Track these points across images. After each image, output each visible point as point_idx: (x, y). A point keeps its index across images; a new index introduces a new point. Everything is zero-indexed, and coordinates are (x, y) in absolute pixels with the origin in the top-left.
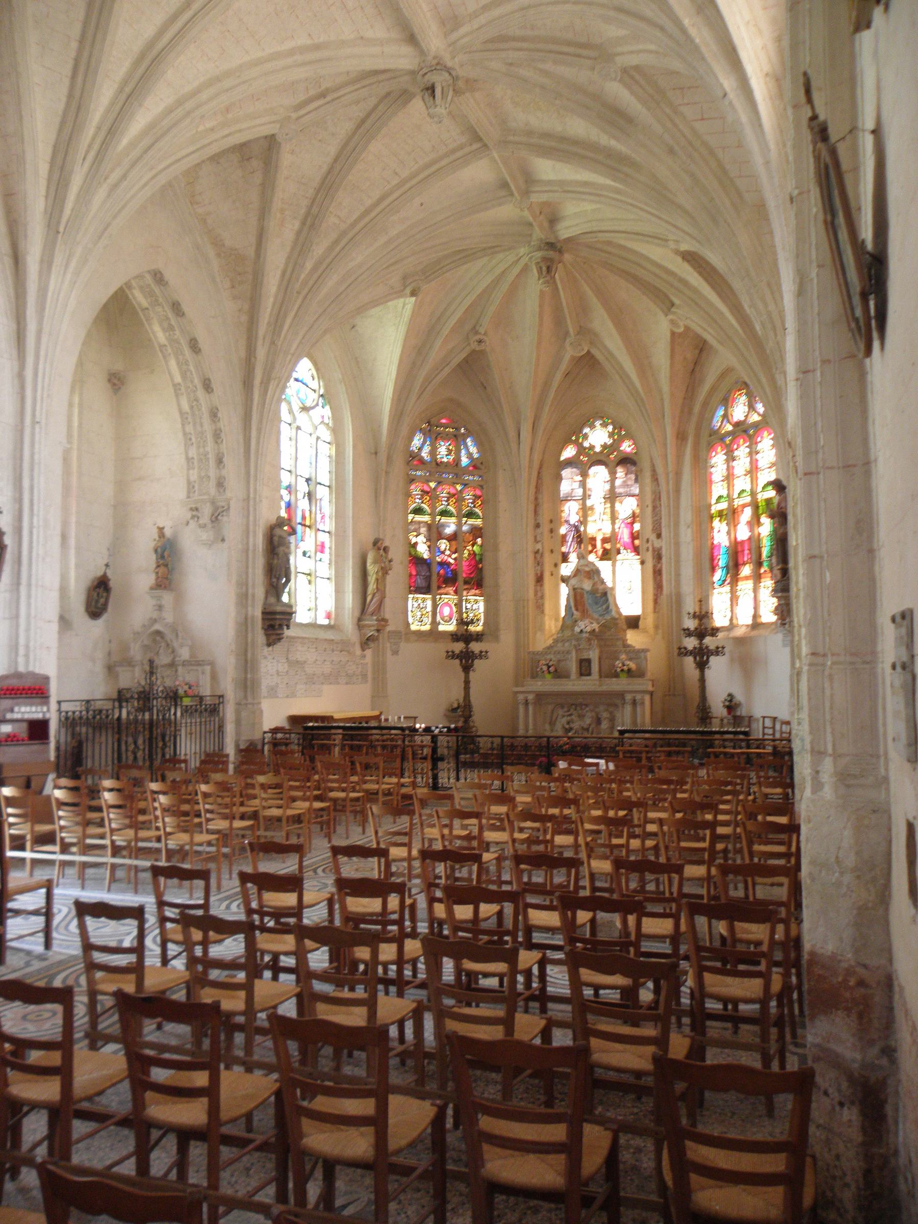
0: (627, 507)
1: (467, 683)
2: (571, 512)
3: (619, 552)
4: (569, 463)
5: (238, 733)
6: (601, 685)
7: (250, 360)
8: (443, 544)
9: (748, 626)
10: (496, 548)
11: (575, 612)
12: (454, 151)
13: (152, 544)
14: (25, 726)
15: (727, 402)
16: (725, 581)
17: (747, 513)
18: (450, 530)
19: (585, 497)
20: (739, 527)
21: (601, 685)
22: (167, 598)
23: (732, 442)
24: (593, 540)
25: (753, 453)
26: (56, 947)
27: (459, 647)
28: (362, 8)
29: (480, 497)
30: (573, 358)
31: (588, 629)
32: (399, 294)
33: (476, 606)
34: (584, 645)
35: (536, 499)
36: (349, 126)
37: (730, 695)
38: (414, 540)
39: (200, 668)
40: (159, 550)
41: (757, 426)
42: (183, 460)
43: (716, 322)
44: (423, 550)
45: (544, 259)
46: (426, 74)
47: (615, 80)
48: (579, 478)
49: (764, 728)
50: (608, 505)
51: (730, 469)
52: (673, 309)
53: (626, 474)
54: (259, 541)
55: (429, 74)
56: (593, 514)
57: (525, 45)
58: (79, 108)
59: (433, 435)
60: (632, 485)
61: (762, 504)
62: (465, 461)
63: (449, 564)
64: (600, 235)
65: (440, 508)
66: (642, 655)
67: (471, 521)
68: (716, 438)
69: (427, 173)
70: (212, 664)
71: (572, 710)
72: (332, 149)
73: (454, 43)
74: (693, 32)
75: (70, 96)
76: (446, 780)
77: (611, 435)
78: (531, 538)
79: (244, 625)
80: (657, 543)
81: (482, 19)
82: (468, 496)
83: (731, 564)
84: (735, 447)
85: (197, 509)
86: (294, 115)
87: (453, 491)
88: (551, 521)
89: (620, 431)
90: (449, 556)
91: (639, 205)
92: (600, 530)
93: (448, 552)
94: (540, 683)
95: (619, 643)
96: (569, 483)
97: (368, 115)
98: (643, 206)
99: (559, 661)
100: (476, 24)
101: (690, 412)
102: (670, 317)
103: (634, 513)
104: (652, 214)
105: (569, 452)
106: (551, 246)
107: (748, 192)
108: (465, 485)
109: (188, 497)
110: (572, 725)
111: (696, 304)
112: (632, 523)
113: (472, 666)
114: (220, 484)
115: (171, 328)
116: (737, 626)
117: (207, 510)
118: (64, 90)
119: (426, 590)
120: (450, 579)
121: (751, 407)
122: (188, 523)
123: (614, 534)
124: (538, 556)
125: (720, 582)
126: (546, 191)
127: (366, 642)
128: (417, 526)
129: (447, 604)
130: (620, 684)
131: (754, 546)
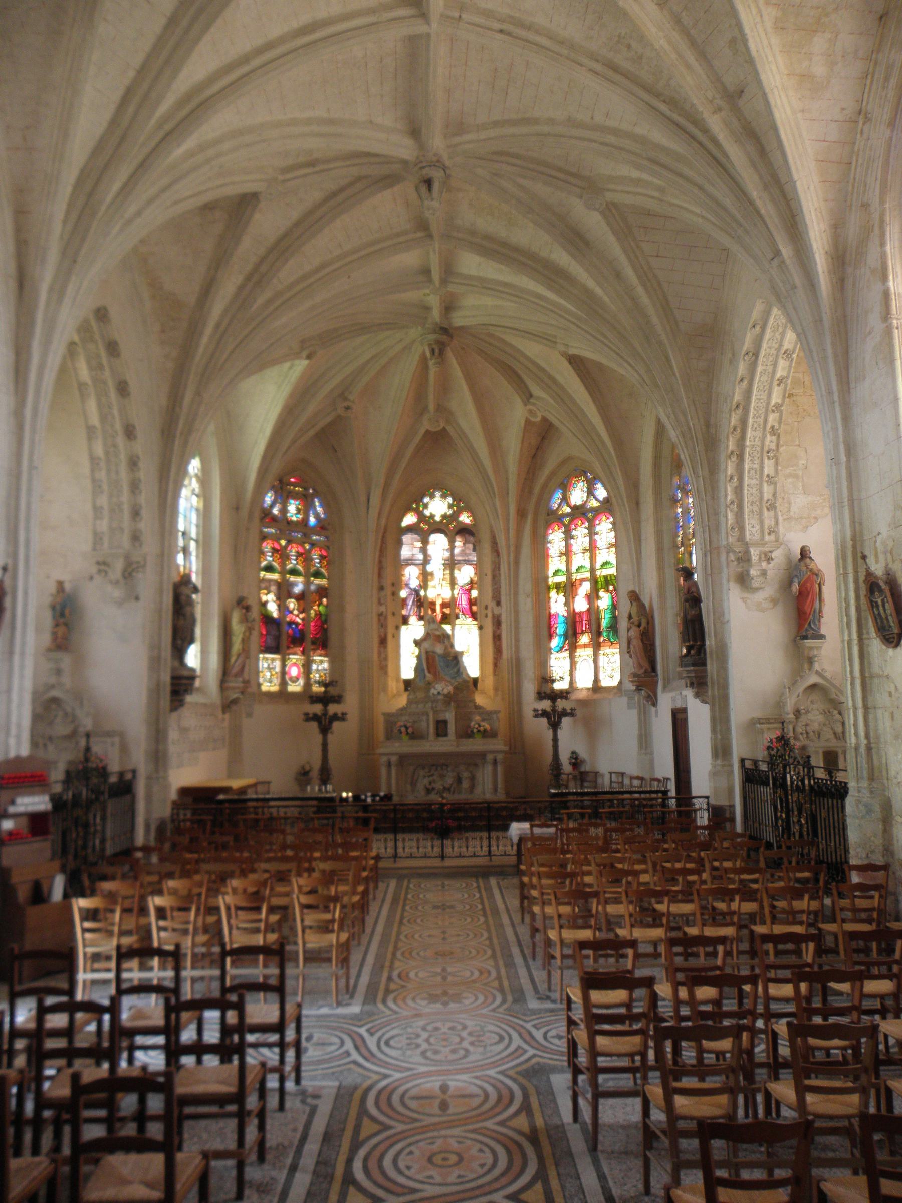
0: (466, 574)
1: (325, 745)
2: (411, 575)
4: (410, 529)
5: (148, 811)
6: (457, 746)
8: (292, 604)
9: (588, 689)
10: (342, 609)
11: (428, 675)
12: (398, 235)
13: (48, 600)
14: (24, 821)
15: (565, 487)
16: (563, 647)
17: (586, 588)
18: (297, 590)
19: (426, 561)
20: (577, 599)
21: (457, 746)
22: (66, 661)
23: (571, 522)
24: (433, 604)
25: (592, 533)
26: (304, 1082)
27: (318, 708)
28: (382, 96)
29: (325, 557)
30: (428, 432)
31: (446, 691)
32: (297, 356)
33: (321, 665)
35: (380, 562)
36: (317, 196)
37: (573, 753)
38: (264, 598)
39: (109, 740)
40: (58, 607)
41: (597, 512)
42: (89, 507)
43: (577, 417)
44: (273, 608)
45: (438, 342)
46: (424, 168)
47: (597, 210)
48: (419, 544)
49: (611, 782)
50: (448, 572)
51: (568, 547)
52: (531, 400)
54: (168, 600)
56: (432, 579)
57: (518, 162)
58: (123, 138)
59: (283, 493)
60: (470, 555)
61: (601, 581)
62: (312, 521)
63: (297, 624)
64: (491, 328)
65: (289, 567)
66: (494, 716)
67: (318, 582)
68: (554, 518)
70: (122, 735)
71: (433, 772)
72: (295, 214)
74: (759, 203)
75: (114, 122)
77: (450, 506)
78: (375, 600)
79: (155, 692)
80: (497, 611)
81: (492, 133)
82: (315, 556)
83: (570, 632)
84: (573, 527)
85: (104, 563)
86: (280, 178)
87: (300, 550)
88: (393, 585)
89: (460, 503)
90: (297, 616)
91: (560, 312)
92: (439, 595)
93: (296, 612)
94: (397, 745)
96: (409, 548)
97: (342, 190)
98: (563, 314)
99: (414, 722)
100: (483, 135)
101: (530, 492)
102: (530, 407)
106: (445, 331)
107: (683, 321)
108: (313, 545)
109: (94, 549)
110: (434, 785)
111: (562, 400)
112: (469, 591)
114: (136, 538)
115: (101, 367)
116: (577, 689)
117: (119, 566)
118: (107, 115)
119: (275, 649)
121: (591, 492)
122: (91, 578)
123: (453, 599)
124: (382, 618)
125: (558, 648)
126: (464, 284)
127: (228, 706)
128: (267, 584)
129: (295, 664)
130: (475, 745)
131: (593, 617)
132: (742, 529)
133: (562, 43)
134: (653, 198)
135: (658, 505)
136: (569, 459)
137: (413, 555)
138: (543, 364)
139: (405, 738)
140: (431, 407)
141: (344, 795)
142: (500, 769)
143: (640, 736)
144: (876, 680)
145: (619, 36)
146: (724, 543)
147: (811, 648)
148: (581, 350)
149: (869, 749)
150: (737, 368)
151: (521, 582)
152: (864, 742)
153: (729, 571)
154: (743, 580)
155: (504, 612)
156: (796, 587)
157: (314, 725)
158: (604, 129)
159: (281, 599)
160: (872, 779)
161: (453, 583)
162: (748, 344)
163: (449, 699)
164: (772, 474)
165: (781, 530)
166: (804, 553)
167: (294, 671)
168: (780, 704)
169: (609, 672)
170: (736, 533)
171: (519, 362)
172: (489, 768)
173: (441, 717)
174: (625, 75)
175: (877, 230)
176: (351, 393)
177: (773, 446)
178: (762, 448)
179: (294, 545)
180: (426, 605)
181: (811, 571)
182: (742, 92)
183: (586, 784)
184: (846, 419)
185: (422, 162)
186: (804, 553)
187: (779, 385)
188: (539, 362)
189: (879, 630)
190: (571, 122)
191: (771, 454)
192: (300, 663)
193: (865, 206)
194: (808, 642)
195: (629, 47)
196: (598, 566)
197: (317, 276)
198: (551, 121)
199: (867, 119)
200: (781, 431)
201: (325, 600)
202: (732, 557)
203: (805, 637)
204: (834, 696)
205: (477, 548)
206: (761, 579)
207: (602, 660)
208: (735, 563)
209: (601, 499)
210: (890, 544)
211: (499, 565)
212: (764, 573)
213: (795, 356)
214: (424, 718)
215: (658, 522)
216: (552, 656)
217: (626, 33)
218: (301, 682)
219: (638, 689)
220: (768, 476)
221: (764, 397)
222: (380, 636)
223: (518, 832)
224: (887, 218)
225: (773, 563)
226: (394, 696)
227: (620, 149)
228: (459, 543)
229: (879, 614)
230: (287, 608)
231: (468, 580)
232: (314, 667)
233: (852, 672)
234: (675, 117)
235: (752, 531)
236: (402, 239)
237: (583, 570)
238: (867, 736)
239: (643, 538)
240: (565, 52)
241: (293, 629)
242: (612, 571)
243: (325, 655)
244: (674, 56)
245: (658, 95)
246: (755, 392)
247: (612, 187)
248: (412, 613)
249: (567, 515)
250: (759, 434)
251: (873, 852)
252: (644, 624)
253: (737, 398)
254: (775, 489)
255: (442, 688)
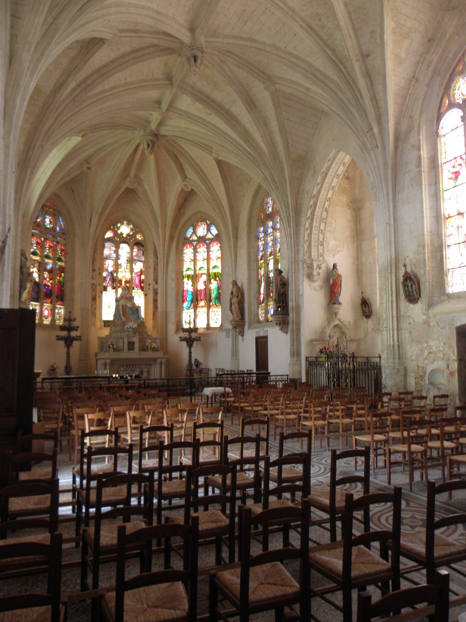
0: (138, 267)
2: (109, 265)
3: (134, 289)
4: (109, 240)
7: (28, 152)
8: (46, 275)
9: (204, 328)
10: (73, 280)
11: (123, 318)
12: (155, 80)
17: (204, 278)
18: (49, 267)
19: (118, 258)
21: (139, 355)
23: (197, 245)
24: (120, 281)
27: (65, 333)
28: (185, 6)
31: (134, 327)
32: (77, 134)
33: (61, 311)
34: (131, 334)
35: (94, 256)
36: (127, 49)
38: (32, 270)
41: (212, 240)
45: (151, 141)
46: (194, 49)
47: (269, 91)
48: (114, 248)
50: (129, 265)
51: (208, 256)
52: (186, 180)
53: (138, 251)
55: (196, 50)
56: (121, 267)
57: (237, 59)
60: (141, 256)
63: (48, 286)
67: (59, 263)
68: (188, 241)
69: (140, 84)
71: (128, 368)
73: (210, 42)
76: (200, 401)
77: (132, 230)
78: (91, 277)
80: (156, 287)
81: (231, 41)
83: (195, 299)
86: (119, 34)
87: (51, 245)
88: (100, 269)
89: (136, 229)
90: (49, 282)
92: (124, 277)
93: (48, 279)
94: (107, 354)
95: (145, 334)
96: (108, 250)
100: (226, 41)
101: (176, 227)
103: (141, 270)
104: (232, 144)
105: (109, 234)
108: (58, 243)
112: (140, 276)
113: (72, 344)
120: (48, 295)
121: (209, 230)
124: (94, 287)
125: (187, 308)
129: (47, 309)
130: (148, 355)
132: (310, 253)
133: (289, 8)
134: (302, 92)
135: (249, 240)
136: (199, 212)
137: (110, 254)
138: (198, 162)
139: (112, 350)
140: (132, 175)
141: (114, 376)
142: (163, 366)
143: (233, 351)
144: (402, 318)
145: (317, 13)
146: (302, 259)
147: (336, 309)
148: (225, 157)
149: (399, 346)
150: (317, 179)
151: (169, 273)
152: (396, 343)
153: (303, 272)
154: (310, 276)
155: (160, 288)
156: (331, 281)
157: (62, 343)
158: (290, 54)
159: (40, 272)
160: (399, 358)
161: (132, 271)
162: (324, 169)
163: (135, 331)
164: (323, 229)
165: (325, 255)
166: (335, 266)
167: (46, 313)
168: (323, 332)
169: (215, 320)
170: (308, 255)
171: (187, 159)
172: (158, 366)
173: (131, 340)
174: (315, 32)
175: (416, 128)
176: (92, 160)
177: (325, 217)
178: (321, 217)
179: (48, 241)
180: (117, 281)
181: (338, 274)
182: (369, 55)
183: (202, 375)
184: (394, 207)
185: (193, 46)
186: (335, 266)
187: (332, 189)
188: (196, 160)
189: (407, 296)
190: (273, 46)
191: (324, 220)
192: (49, 308)
193: (411, 117)
194: (336, 306)
195: (320, 20)
196: (211, 267)
197: (111, 93)
198: (264, 43)
199: (417, 81)
200: (329, 210)
201: (63, 274)
202: (305, 265)
203: (335, 304)
204: (344, 330)
205: (145, 254)
206: (317, 276)
207: (211, 314)
208: (306, 268)
209: (214, 234)
210: (414, 261)
211: (158, 263)
212: (319, 274)
213: (341, 177)
214: (121, 341)
215: (249, 248)
216: (184, 311)
217: (321, 13)
218: (50, 319)
219: (235, 327)
220: (322, 230)
221: (325, 194)
222: (92, 296)
223: (212, 392)
224: (421, 125)
225: (321, 270)
226: (99, 329)
227: (298, 65)
228: (135, 250)
229: (408, 290)
230: (43, 277)
231: (139, 270)
232: (57, 311)
233: (392, 314)
234: (334, 58)
235: (314, 254)
236: (158, 83)
237: (203, 269)
238: (398, 341)
239: (238, 255)
240: (290, 13)
241: (46, 289)
242: (219, 270)
243: (62, 305)
244: (346, 31)
245: (328, 46)
246: (322, 191)
247: (280, 82)
248: (109, 285)
249: (195, 241)
250: (320, 210)
251: (399, 388)
252: (240, 297)
253: (315, 192)
254: (324, 236)
255: (132, 324)
